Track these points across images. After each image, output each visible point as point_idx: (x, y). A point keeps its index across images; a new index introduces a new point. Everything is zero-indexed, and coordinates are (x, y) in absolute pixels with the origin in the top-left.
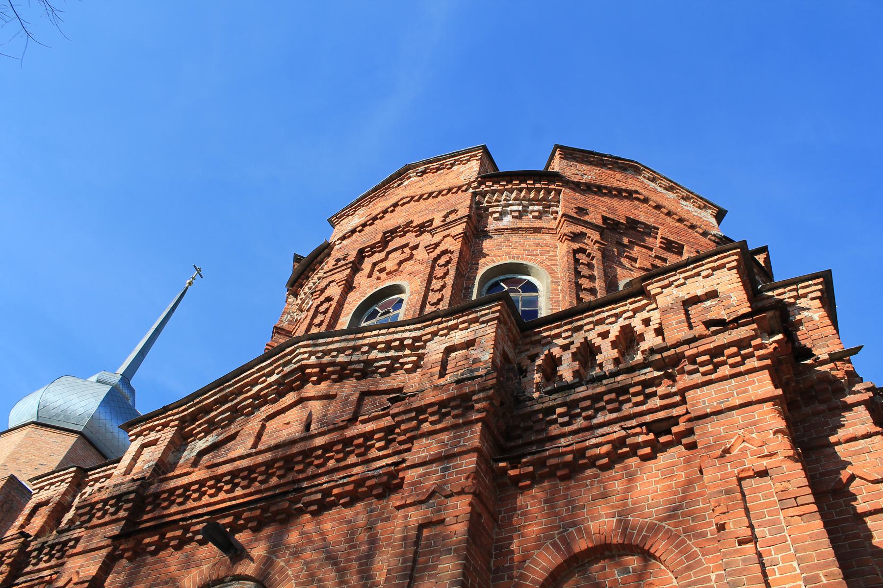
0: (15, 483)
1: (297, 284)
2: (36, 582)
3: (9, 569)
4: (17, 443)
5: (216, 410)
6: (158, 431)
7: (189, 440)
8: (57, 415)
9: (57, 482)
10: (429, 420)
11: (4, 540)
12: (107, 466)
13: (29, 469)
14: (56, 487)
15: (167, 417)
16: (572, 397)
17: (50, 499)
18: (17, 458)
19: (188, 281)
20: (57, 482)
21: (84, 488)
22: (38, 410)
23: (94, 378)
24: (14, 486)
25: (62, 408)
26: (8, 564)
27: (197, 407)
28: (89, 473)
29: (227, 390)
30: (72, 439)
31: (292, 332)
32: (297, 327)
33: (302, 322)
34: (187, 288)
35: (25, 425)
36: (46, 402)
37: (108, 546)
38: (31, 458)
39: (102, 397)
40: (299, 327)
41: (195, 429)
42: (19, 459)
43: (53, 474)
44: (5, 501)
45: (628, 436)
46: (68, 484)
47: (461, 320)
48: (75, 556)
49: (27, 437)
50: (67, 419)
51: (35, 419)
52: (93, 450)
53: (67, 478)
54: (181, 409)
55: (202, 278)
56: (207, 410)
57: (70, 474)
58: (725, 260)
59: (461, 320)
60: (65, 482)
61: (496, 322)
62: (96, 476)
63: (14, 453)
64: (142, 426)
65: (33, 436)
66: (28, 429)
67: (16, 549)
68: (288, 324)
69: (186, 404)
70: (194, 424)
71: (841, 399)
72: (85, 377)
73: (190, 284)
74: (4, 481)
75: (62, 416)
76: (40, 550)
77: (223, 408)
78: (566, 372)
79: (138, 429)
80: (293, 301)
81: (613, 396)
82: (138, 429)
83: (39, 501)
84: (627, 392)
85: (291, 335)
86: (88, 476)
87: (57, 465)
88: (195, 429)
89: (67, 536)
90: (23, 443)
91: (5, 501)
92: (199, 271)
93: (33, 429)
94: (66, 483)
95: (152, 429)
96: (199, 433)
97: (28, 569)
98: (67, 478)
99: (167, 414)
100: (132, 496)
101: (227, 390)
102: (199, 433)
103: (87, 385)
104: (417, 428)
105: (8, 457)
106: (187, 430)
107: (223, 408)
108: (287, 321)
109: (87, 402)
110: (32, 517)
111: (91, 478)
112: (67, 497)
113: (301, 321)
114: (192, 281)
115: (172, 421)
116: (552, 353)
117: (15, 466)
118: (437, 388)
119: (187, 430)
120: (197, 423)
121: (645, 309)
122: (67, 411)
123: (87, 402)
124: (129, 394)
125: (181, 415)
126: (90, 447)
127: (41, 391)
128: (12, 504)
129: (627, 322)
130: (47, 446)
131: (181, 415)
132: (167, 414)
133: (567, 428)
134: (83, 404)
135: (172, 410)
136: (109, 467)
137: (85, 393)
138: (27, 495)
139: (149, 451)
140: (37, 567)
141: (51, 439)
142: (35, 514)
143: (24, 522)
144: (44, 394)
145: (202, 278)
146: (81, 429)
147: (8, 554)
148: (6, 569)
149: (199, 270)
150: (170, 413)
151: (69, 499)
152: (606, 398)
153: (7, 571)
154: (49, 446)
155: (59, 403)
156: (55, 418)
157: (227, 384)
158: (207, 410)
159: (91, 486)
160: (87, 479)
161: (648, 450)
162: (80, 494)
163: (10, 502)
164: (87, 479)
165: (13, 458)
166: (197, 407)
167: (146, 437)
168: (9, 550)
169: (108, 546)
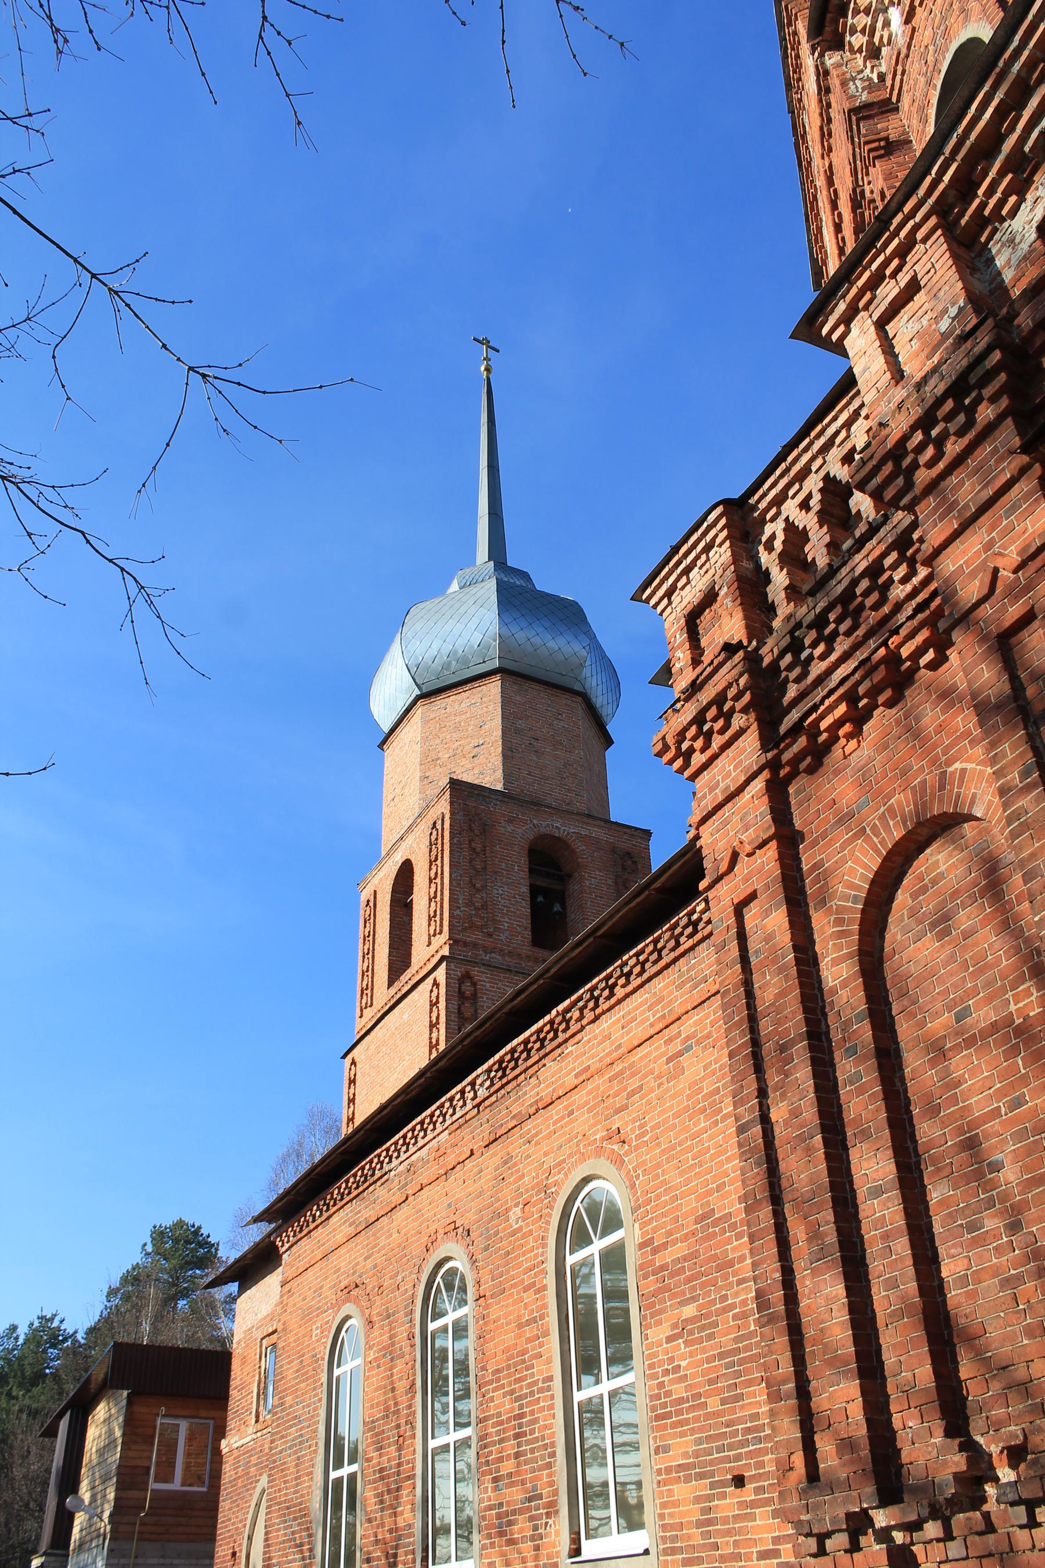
0: (463, 788)
1: (829, 16)
2: (857, 676)
3: (752, 716)
4: (419, 739)
5: (1012, 129)
6: (894, 275)
7: (983, 239)
8: (446, 666)
9: (698, 557)
10: (952, 431)
11: (698, 682)
12: (785, 460)
13: (464, 762)
14: (700, 568)
15: (896, 233)
16: (840, 589)
17: (714, 587)
18: (435, 757)
19: (482, 368)
20: (698, 557)
21: (762, 533)
22: (413, 678)
23: (454, 587)
24: (466, 793)
25: (445, 651)
26: (745, 710)
27: (959, 158)
28: (752, 501)
29: (1016, 67)
30: (493, 688)
31: (890, 99)
32: (898, 77)
33: (907, 56)
34: (488, 379)
35: (408, 710)
36: (417, 658)
37: (1023, 471)
38: (454, 747)
39: (494, 598)
40: (903, 73)
41: (983, 205)
42: (439, 758)
43: (677, 552)
44: (470, 820)
45: (781, 752)
46: (728, 543)
47: (854, 291)
48: (944, 549)
49: (425, 722)
50: (464, 661)
51: (417, 692)
52: (534, 685)
53: (716, 535)
54: (921, 192)
55: (498, 351)
56: (993, 138)
57: (715, 526)
58: (709, 538)
59: (854, 291)
60: (716, 544)
61: (939, 232)
62: (773, 493)
63: (425, 755)
64: (843, 297)
65: (432, 716)
66: (419, 711)
67: (741, 675)
68: (868, 93)
69: (928, 172)
70: (976, 196)
71: (69, 1412)
72: (441, 590)
73: (488, 370)
74: (448, 793)
75: (454, 663)
76: (795, 646)
77: (1027, 114)
78: (817, 551)
79: (842, 306)
80: (842, 58)
81: (839, 609)
82: (842, 306)
83: (690, 608)
84: (911, 543)
85: (893, 106)
86: (754, 507)
87: (500, 733)
88: (983, 205)
89: (840, 582)
90: (428, 734)
91: (470, 820)
92: (485, 342)
93: (426, 707)
94: (720, 545)
95: (877, 280)
96: (1002, 203)
97: (792, 691)
98: (716, 535)
99: (892, 228)
100: (997, 356)
101: (1016, 67)
102: (1002, 203)
103: (457, 598)
104: (909, 485)
105: (421, 765)
106: (963, 222)
107: (1027, 114)
108: (863, 91)
109: (475, 621)
110: (699, 640)
111: (762, 505)
112: (744, 564)
113: (902, 56)
114: (488, 365)
115: (917, 227)
116: (835, 476)
117: (440, 770)
118: (928, 378)
119: (963, 222)
120: (980, 192)
121: (860, 415)
122: (456, 652)
123: (475, 621)
124: (522, 582)
125: (931, 201)
126: (528, 684)
127: (396, 649)
128: (480, 819)
129: (822, 473)
130: (463, 717)
131: (931, 201)
132: (892, 228)
133: (885, 608)
134: (472, 625)
135: (900, 208)
136: (790, 459)
137: (462, 610)
138: (492, 796)
139: (906, 318)
140: (810, 679)
141: (463, 705)
142: (699, 634)
143: (691, 653)
144: (404, 648)
145: (498, 351)
146: (496, 664)
147: (733, 691)
148: (747, 719)
149: (485, 342)
150: (896, 221)
151: (748, 566)
152: (832, 617)
153: (751, 720)
154: (468, 715)
155: (433, 652)
156: (446, 673)
157: (1007, 55)
158: (993, 138)
159: (773, 519)
160: (756, 514)
161: (930, 655)
162: (761, 548)
163: (476, 818)
164: (756, 514)
165: (429, 761)
166: (959, 158)
167: (871, 308)
168: (730, 685)
169: (1023, 471)
